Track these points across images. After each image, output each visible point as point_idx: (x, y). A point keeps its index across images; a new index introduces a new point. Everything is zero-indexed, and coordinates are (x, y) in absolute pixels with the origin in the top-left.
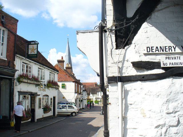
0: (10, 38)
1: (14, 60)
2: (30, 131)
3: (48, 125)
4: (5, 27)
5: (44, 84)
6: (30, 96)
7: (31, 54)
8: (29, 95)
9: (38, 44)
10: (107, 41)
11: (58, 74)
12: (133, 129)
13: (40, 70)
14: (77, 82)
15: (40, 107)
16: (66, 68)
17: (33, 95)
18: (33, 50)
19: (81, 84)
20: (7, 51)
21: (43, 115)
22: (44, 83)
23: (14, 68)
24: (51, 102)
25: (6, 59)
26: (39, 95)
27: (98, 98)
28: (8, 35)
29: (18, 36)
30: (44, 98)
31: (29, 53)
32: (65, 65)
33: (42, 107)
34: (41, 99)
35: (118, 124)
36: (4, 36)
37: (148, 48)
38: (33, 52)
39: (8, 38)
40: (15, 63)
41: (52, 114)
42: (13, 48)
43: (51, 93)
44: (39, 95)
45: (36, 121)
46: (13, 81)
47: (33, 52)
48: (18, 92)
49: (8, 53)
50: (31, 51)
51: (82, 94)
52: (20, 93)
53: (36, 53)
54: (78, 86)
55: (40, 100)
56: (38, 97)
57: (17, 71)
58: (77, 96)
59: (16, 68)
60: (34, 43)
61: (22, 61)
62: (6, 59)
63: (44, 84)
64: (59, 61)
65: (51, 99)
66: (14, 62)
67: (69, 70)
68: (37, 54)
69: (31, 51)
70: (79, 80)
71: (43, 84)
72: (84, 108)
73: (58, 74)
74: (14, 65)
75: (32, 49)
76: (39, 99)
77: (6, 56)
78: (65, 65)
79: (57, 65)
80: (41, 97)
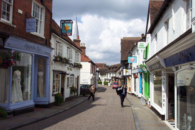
1: (51, 39)
2: (66, 109)
3: (78, 104)
4: (43, 5)
6: (61, 75)
8: (60, 73)
11: (81, 53)
12: (46, 118)
13: (69, 49)
15: (68, 86)
23: (50, 46)
24: (76, 81)
25: (44, 38)
26: (68, 74)
27: (108, 80)
33: (69, 87)
44: (68, 74)
48: (53, 70)
54: (93, 66)
55: (68, 78)
56: (67, 76)
61: (56, 40)
62: (44, 38)
65: (76, 79)
66: (51, 40)
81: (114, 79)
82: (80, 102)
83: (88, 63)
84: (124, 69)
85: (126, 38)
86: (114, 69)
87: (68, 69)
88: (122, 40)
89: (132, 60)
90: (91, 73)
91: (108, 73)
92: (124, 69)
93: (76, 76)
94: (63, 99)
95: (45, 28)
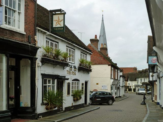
0: (28, 5)
1: (35, 35)
5: (74, 66)
7: (56, 27)
9: (64, 14)
10: (36, 107)
11: (91, 54)
14: (114, 66)
15: (68, 93)
16: (101, 49)
17: (61, 79)
18: (59, 21)
19: (118, 68)
20: (25, 22)
21: (72, 103)
22: (74, 65)
23: (35, 45)
24: (83, 88)
26: (68, 79)
28: (25, 2)
29: (38, 5)
30: (74, 83)
31: (54, 26)
32: (100, 46)
33: (71, 93)
34: (70, 83)
35: (146, 107)
36: (21, 2)
37: (59, 82)
38: (59, 24)
39: (25, 6)
40: (36, 38)
41: (83, 102)
42: (34, 19)
43: (82, 77)
44: (68, 79)
45: (64, 109)
46: (34, 61)
47: (59, 24)
48: (42, 74)
49: (27, 24)
50: (57, 23)
51: (120, 80)
52: (43, 76)
53: (62, 26)
56: (67, 81)
57: (40, 49)
58: (113, 82)
59: (38, 45)
60: (60, 12)
62: (25, 33)
63: (74, 66)
64: (92, 40)
65: (83, 84)
67: (103, 52)
68: (63, 27)
69: (57, 23)
70: (116, 64)
71: (73, 67)
72: (121, 97)
73: (91, 54)
74: (35, 41)
75: (58, 20)
76: (68, 83)
77: (25, 29)
78: (100, 46)
79: (89, 45)
80: (70, 81)
81: (145, 86)
82: (85, 112)
83: (107, 66)
84: (150, 73)
85: (101, 31)
86: (144, 73)
87: (69, 73)
88: (148, 36)
89: (154, 61)
90: (111, 78)
91: (138, 78)
92: (150, 73)
93: (82, 81)
94: (62, 109)
95: (25, 21)
